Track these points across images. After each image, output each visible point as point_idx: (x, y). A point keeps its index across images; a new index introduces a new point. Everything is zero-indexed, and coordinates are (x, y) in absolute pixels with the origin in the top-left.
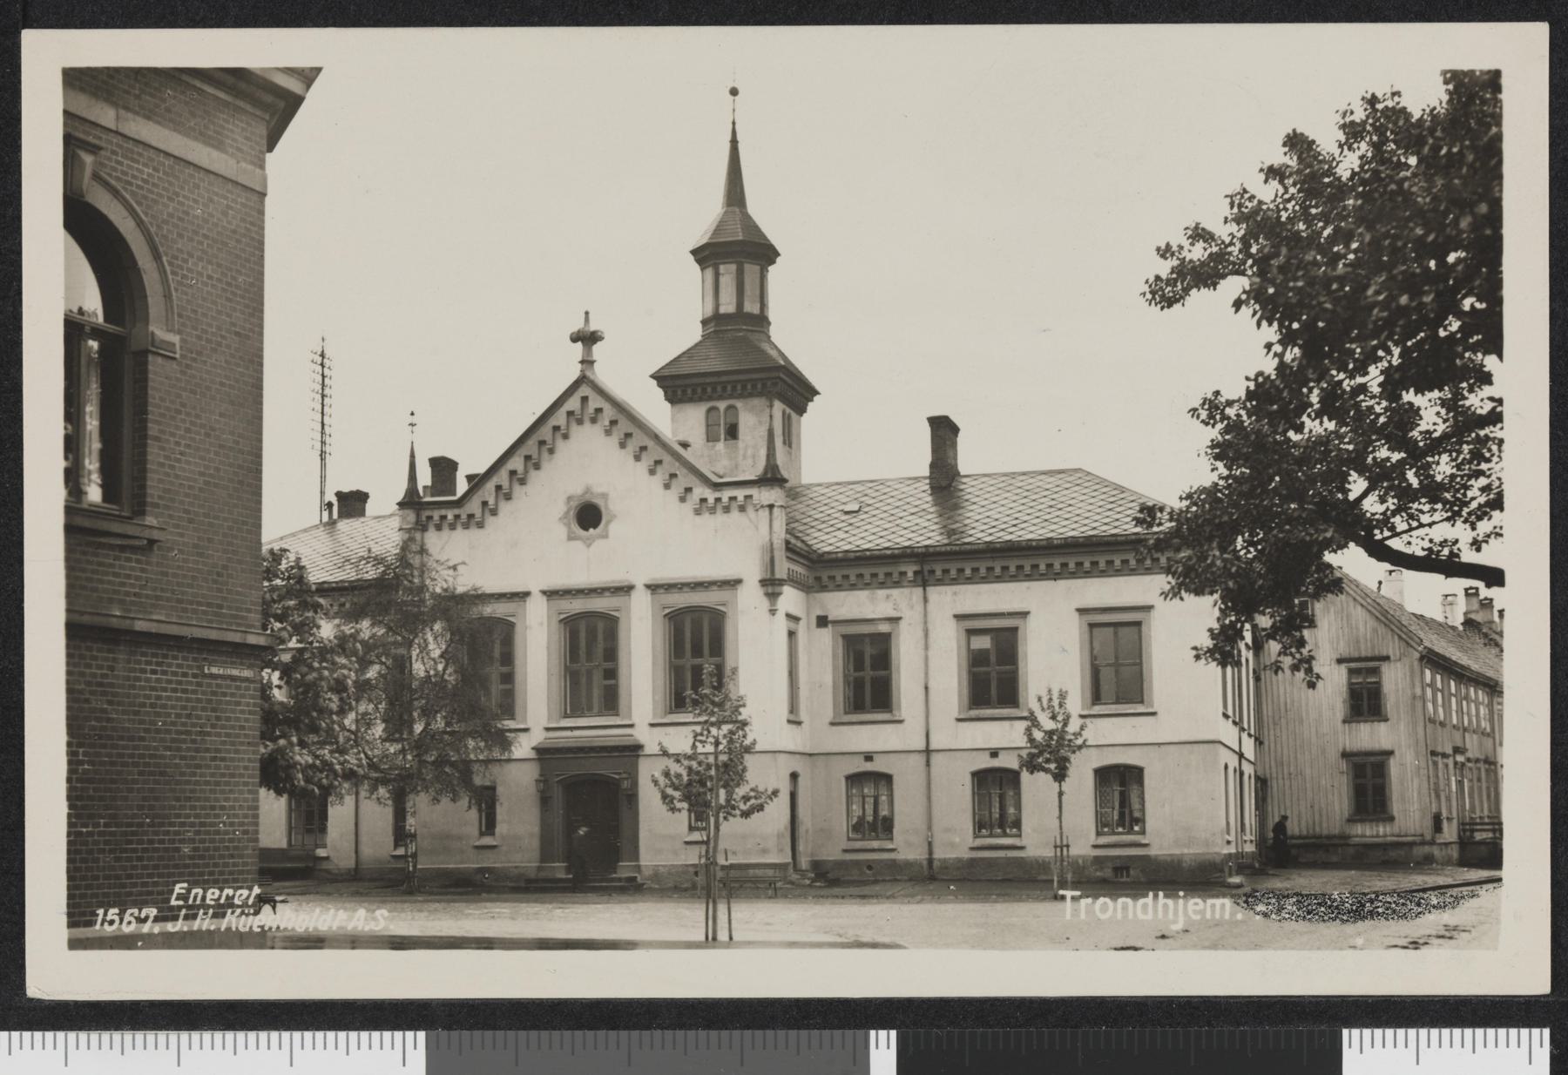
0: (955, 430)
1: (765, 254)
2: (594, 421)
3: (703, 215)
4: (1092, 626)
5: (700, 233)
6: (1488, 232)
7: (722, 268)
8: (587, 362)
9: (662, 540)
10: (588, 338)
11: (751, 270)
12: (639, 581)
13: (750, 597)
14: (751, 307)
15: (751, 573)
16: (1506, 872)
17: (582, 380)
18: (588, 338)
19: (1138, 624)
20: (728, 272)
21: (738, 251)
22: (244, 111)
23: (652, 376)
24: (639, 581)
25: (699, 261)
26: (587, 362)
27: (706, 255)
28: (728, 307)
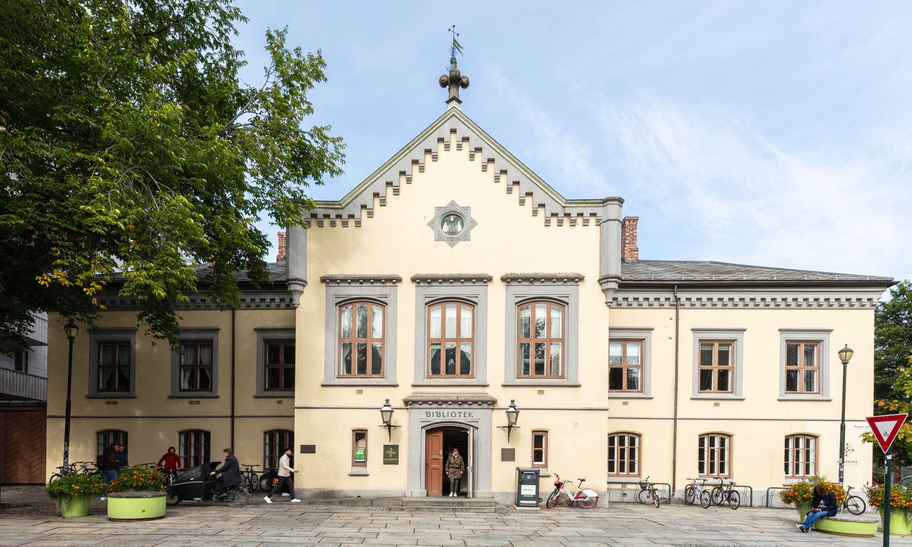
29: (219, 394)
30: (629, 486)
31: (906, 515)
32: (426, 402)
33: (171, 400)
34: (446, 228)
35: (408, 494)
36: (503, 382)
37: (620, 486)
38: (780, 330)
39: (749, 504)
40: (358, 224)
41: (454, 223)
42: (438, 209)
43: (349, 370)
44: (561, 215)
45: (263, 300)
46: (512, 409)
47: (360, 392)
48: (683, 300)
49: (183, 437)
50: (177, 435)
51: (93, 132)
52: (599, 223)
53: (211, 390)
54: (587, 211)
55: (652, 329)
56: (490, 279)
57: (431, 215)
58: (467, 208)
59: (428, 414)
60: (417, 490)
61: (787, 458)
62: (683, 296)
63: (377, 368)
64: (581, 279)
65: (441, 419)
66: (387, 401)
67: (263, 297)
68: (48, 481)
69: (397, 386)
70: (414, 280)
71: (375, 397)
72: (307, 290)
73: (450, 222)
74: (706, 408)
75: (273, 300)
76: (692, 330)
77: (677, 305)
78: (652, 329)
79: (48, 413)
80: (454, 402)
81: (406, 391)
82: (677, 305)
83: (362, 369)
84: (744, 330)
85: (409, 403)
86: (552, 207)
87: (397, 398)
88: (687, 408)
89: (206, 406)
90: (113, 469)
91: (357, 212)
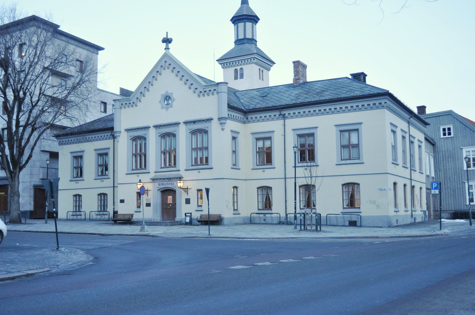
0: (305, 67)
1: (254, 19)
2: (168, 68)
3: (234, 6)
4: (341, 131)
5: (232, 14)
6: (54, 210)
7: (239, 24)
8: (167, 48)
9: (190, 107)
10: (167, 41)
11: (249, 25)
12: (181, 122)
13: (214, 127)
14: (249, 36)
15: (215, 118)
16: (231, 22)
17: (165, 55)
18: (167, 41)
19: (357, 130)
20: (241, 25)
21: (245, 18)
22: (431, 139)
23: (217, 60)
24: (181, 122)
25: (233, 23)
26: (167, 48)
27: (236, 20)
28: (241, 37)
30: (267, 215)
31: (5, 216)
32: (160, 179)
34: (166, 102)
35: (153, 220)
36: (185, 168)
37: (262, 215)
38: (335, 126)
39: (325, 223)
40: (136, 106)
41: (168, 100)
42: (162, 95)
44: (203, 92)
49: (100, 197)
50: (97, 196)
52: (218, 93)
54: (212, 89)
55: (274, 131)
56: (180, 123)
57: (159, 98)
58: (172, 94)
59: (159, 184)
60: (158, 218)
61: (295, 199)
62: (286, 112)
64: (212, 119)
65: (163, 186)
66: (140, 180)
69: (149, 173)
70: (154, 126)
71: (142, 177)
72: (121, 134)
73: (167, 100)
76: (293, 130)
77: (284, 117)
78: (274, 131)
79: (59, 188)
80: (167, 179)
81: (152, 175)
82: (284, 117)
84: (317, 127)
85: (154, 180)
86: (200, 89)
90: (315, 209)
91: (135, 101)
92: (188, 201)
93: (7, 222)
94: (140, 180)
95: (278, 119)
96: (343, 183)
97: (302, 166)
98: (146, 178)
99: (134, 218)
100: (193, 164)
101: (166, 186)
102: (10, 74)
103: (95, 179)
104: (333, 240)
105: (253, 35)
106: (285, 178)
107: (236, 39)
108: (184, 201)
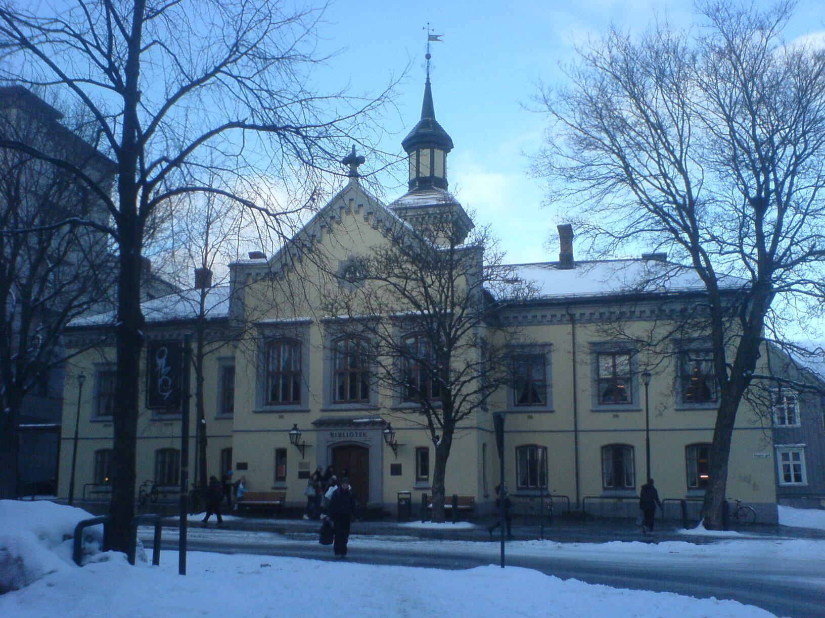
29: (554, 408)
33: (596, 414)
43: (342, 396)
45: (535, 317)
46: (295, 432)
47: (281, 417)
48: (577, 316)
51: (408, 218)
53: (545, 405)
59: (332, 435)
62: (577, 312)
63: (297, 398)
65: (342, 439)
67: (525, 314)
68: (137, 490)
71: (290, 420)
74: (605, 420)
75: (544, 316)
81: (316, 414)
82: (573, 320)
83: (353, 395)
85: (320, 424)
87: (305, 421)
88: (588, 420)
89: (540, 421)
92: (396, 470)
93: (689, 398)
94: (295, 425)
95: (560, 322)
96: (689, 442)
97: (609, 411)
98: (305, 421)
99: (287, 500)
100: (337, 399)
101: (349, 439)
102: (201, 235)
103: (255, 412)
104: (695, 559)
105: (445, 173)
106: (576, 431)
107: (414, 176)
108: (387, 469)
